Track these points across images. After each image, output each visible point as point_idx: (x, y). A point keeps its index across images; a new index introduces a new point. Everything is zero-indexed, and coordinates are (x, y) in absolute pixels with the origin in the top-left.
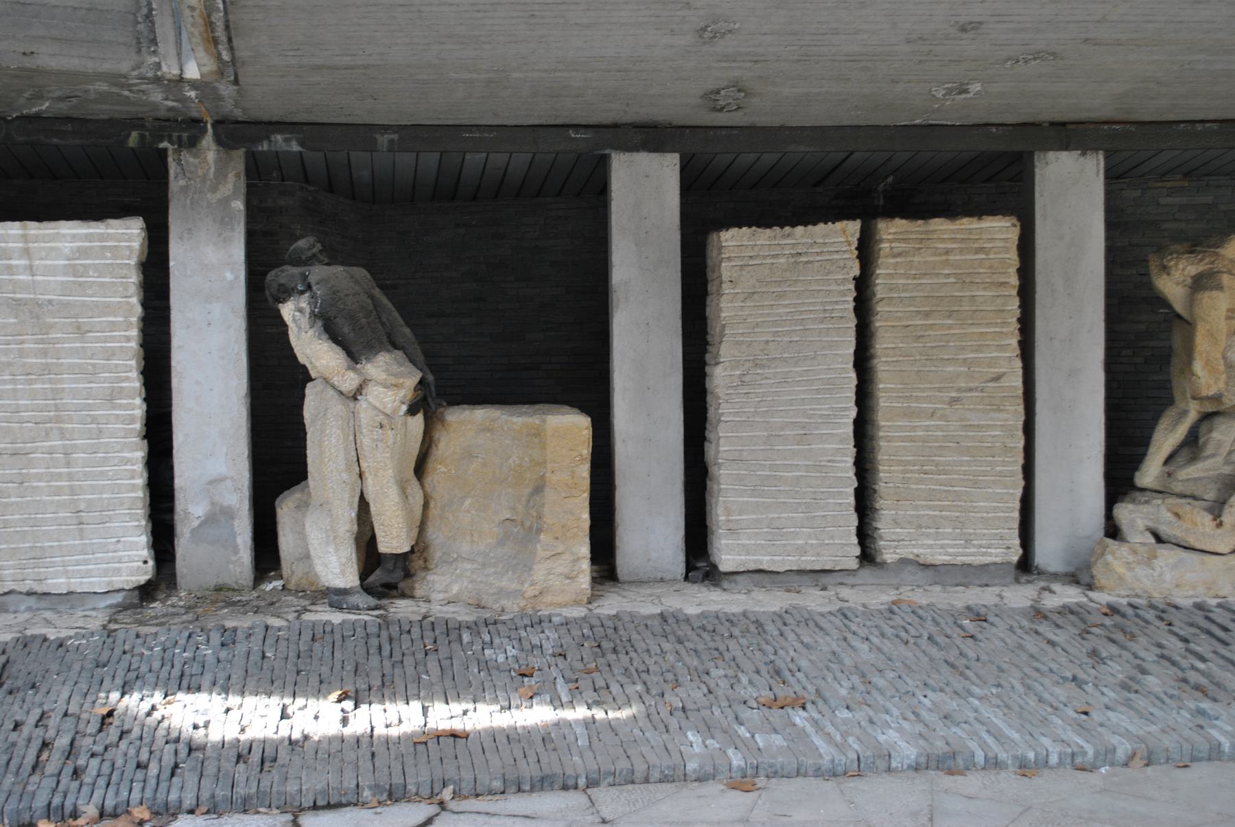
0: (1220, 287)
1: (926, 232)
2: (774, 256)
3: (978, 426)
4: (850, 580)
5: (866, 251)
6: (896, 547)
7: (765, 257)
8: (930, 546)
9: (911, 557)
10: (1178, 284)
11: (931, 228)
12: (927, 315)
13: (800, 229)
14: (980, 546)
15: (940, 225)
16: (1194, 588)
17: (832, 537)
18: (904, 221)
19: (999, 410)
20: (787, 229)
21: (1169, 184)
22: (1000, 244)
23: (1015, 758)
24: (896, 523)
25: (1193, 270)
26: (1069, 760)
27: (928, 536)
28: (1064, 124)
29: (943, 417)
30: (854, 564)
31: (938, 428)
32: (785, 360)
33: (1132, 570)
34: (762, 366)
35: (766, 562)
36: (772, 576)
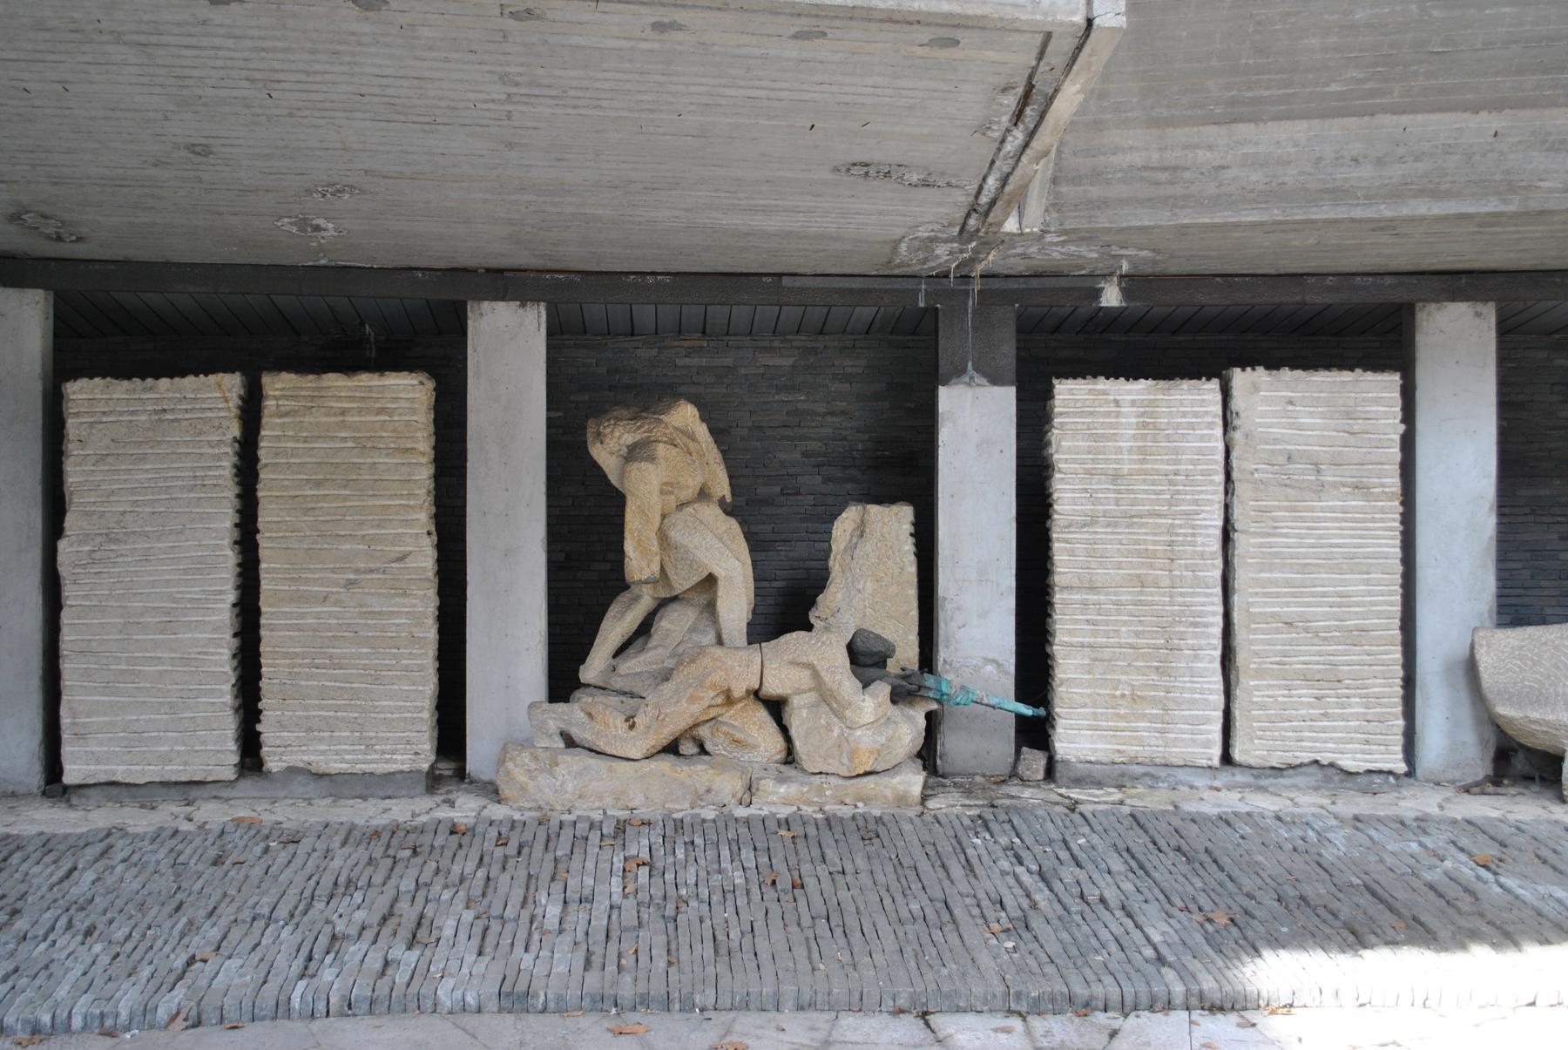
0: (652, 459)
1: (319, 389)
2: (132, 413)
3: (379, 613)
4: (225, 793)
5: (251, 412)
6: (282, 754)
7: (121, 413)
8: (323, 753)
9: (301, 765)
10: (611, 453)
11: (325, 384)
12: (318, 484)
13: (164, 382)
14: (383, 752)
15: (334, 381)
16: (601, 799)
17: (204, 743)
18: (293, 376)
19: (405, 595)
20: (149, 381)
21: (686, 344)
22: (407, 405)
23: (25, 1022)
24: (281, 725)
25: (629, 439)
26: (96, 1023)
27: (321, 740)
28: (501, 271)
29: (337, 603)
30: (230, 774)
31: (331, 615)
32: (146, 535)
33: (534, 778)
34: (118, 541)
35: (120, 773)
36: (133, 789)
